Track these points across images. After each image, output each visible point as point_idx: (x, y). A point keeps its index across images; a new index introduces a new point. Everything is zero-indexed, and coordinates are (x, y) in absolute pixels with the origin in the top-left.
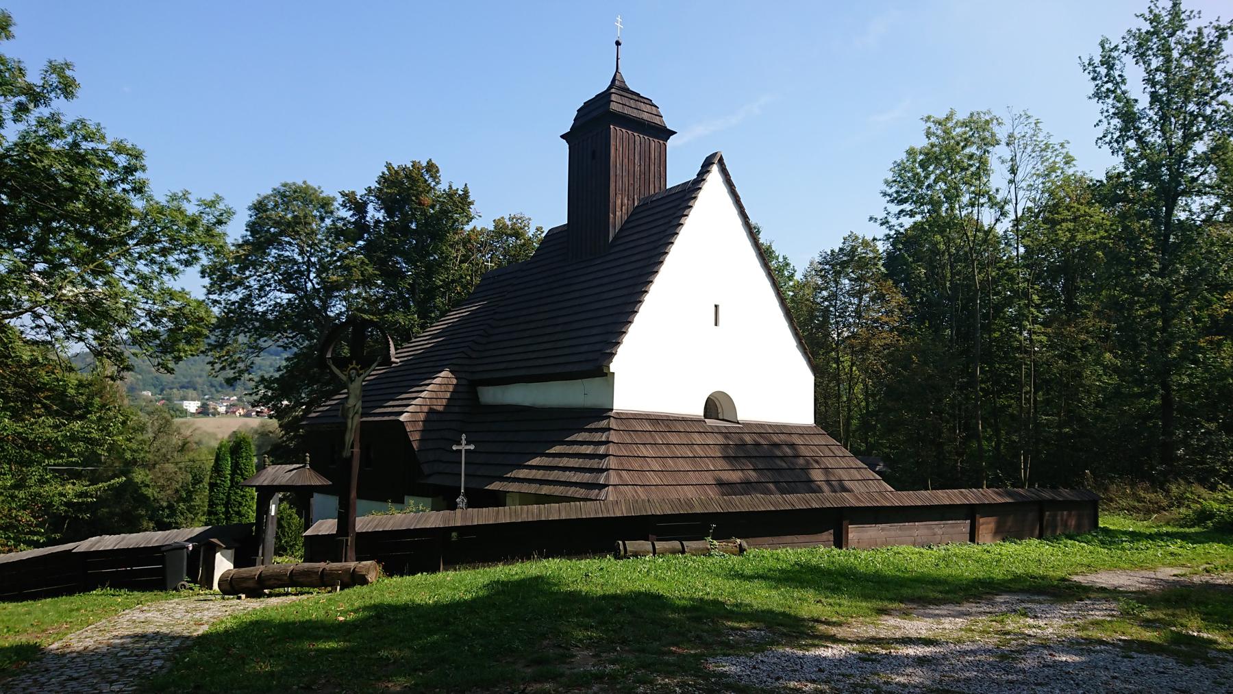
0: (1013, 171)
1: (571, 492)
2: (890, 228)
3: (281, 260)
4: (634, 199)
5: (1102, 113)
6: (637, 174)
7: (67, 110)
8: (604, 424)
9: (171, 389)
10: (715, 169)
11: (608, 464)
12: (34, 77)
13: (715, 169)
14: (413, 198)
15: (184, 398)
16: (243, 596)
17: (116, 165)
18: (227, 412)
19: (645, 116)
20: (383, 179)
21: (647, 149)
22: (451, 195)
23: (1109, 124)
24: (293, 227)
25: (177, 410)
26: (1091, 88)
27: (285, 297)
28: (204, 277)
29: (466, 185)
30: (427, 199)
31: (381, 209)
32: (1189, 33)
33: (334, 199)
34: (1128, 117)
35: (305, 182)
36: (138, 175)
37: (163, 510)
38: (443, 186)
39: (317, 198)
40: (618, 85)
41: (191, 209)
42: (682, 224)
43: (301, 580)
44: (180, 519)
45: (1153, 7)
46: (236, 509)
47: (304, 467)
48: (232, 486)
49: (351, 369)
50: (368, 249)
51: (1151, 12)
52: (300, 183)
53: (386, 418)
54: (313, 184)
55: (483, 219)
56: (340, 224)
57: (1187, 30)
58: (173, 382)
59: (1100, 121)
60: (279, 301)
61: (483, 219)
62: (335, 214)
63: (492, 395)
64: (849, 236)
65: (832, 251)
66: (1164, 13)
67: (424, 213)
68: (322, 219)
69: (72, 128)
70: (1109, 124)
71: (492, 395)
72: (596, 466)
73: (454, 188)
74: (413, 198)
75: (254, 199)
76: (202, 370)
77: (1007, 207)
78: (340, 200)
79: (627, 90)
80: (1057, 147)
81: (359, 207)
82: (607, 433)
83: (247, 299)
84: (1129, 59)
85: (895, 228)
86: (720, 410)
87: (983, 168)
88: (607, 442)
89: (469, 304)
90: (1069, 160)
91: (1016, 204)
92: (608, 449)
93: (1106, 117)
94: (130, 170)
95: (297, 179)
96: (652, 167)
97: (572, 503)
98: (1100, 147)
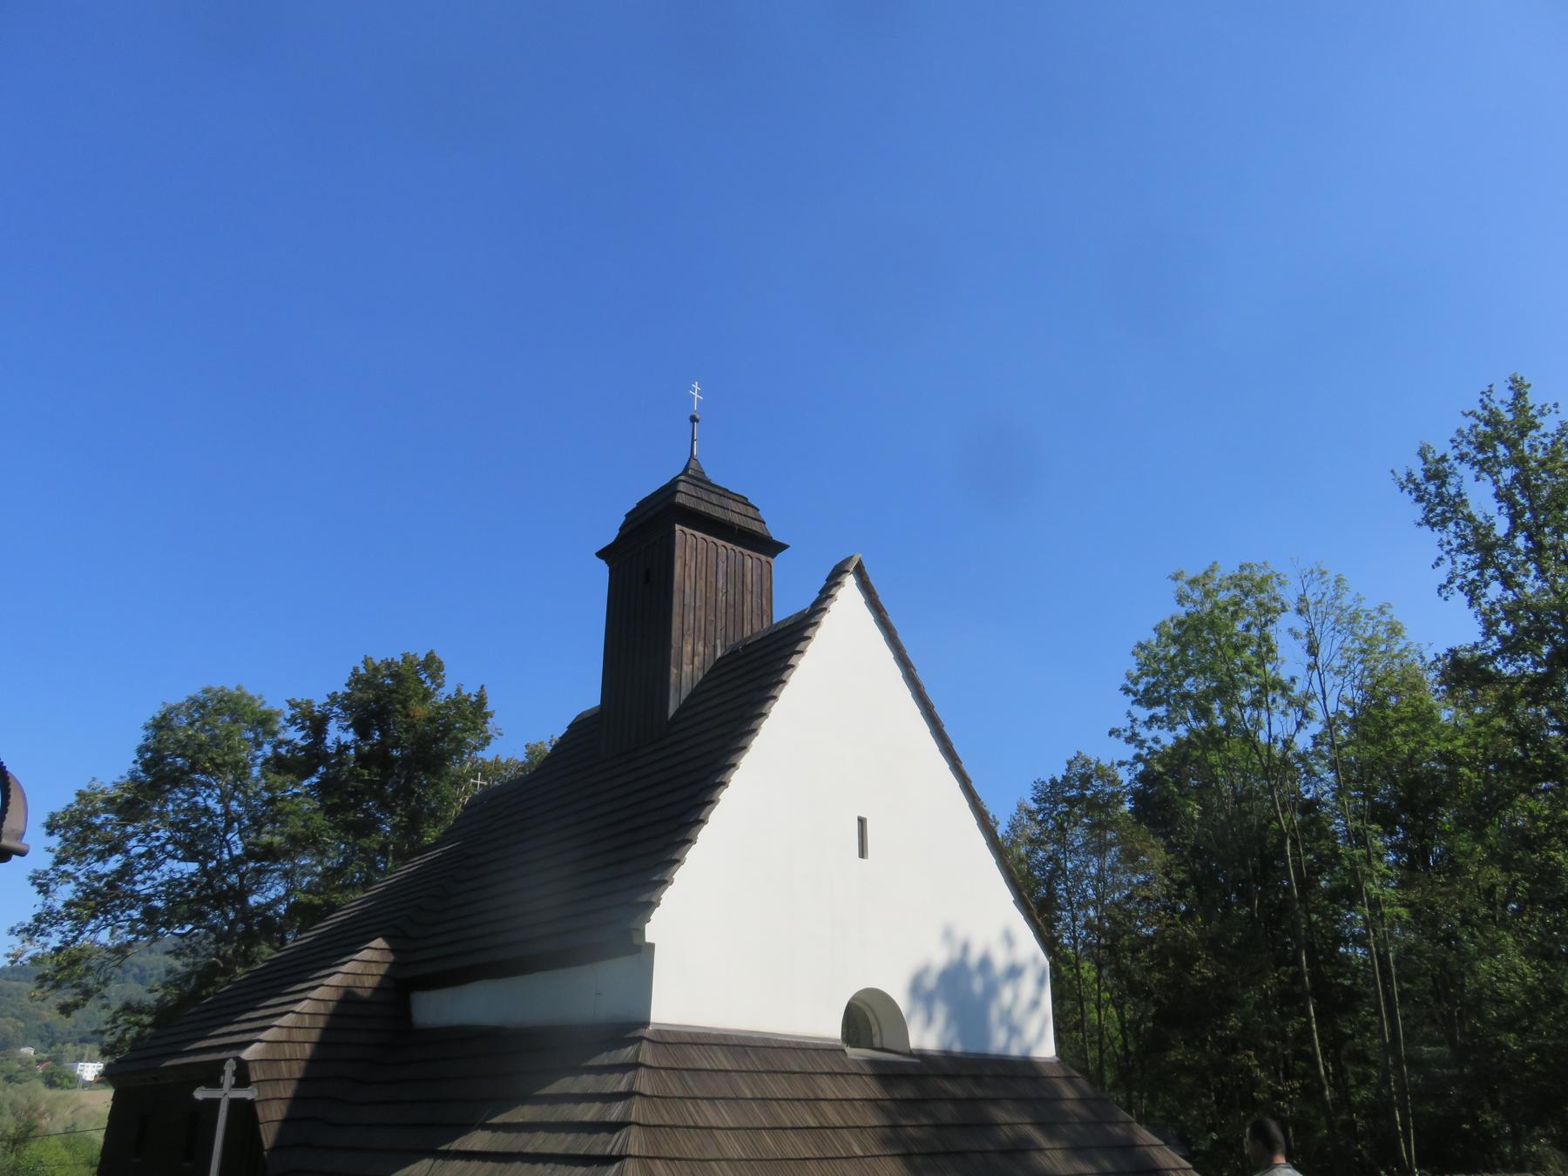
0: (1312, 650)
2: (1141, 744)
4: (715, 647)
5: (1441, 546)
6: (722, 606)
8: (627, 1054)
9: (64, 1043)
10: (850, 581)
11: (625, 1144)
13: (850, 581)
14: (398, 706)
15: (80, 1058)
19: (736, 519)
20: (356, 680)
21: (738, 568)
22: (457, 702)
23: (1454, 562)
25: (66, 1076)
26: (1418, 511)
28: (51, 834)
29: (482, 687)
30: (420, 711)
32: (1545, 435)
33: (278, 714)
34: (1484, 547)
35: (238, 688)
39: (253, 713)
42: (793, 666)
45: (1486, 400)
50: (324, 787)
51: (1484, 407)
54: (251, 690)
57: (1542, 430)
59: (1440, 559)
64: (1076, 758)
65: (1053, 781)
66: (1503, 409)
68: (259, 745)
70: (1454, 562)
72: (597, 1151)
73: (465, 692)
74: (398, 706)
75: (155, 711)
77: (1310, 705)
79: (709, 483)
80: (1374, 614)
81: (317, 726)
82: (630, 1074)
83: (126, 872)
84: (1464, 470)
85: (1147, 745)
86: (875, 1029)
87: (1266, 649)
88: (628, 1095)
89: (433, 850)
90: (1394, 631)
91: (1324, 699)
92: (627, 1111)
93: (1448, 553)
95: (226, 680)
96: (748, 598)
98: (1446, 599)
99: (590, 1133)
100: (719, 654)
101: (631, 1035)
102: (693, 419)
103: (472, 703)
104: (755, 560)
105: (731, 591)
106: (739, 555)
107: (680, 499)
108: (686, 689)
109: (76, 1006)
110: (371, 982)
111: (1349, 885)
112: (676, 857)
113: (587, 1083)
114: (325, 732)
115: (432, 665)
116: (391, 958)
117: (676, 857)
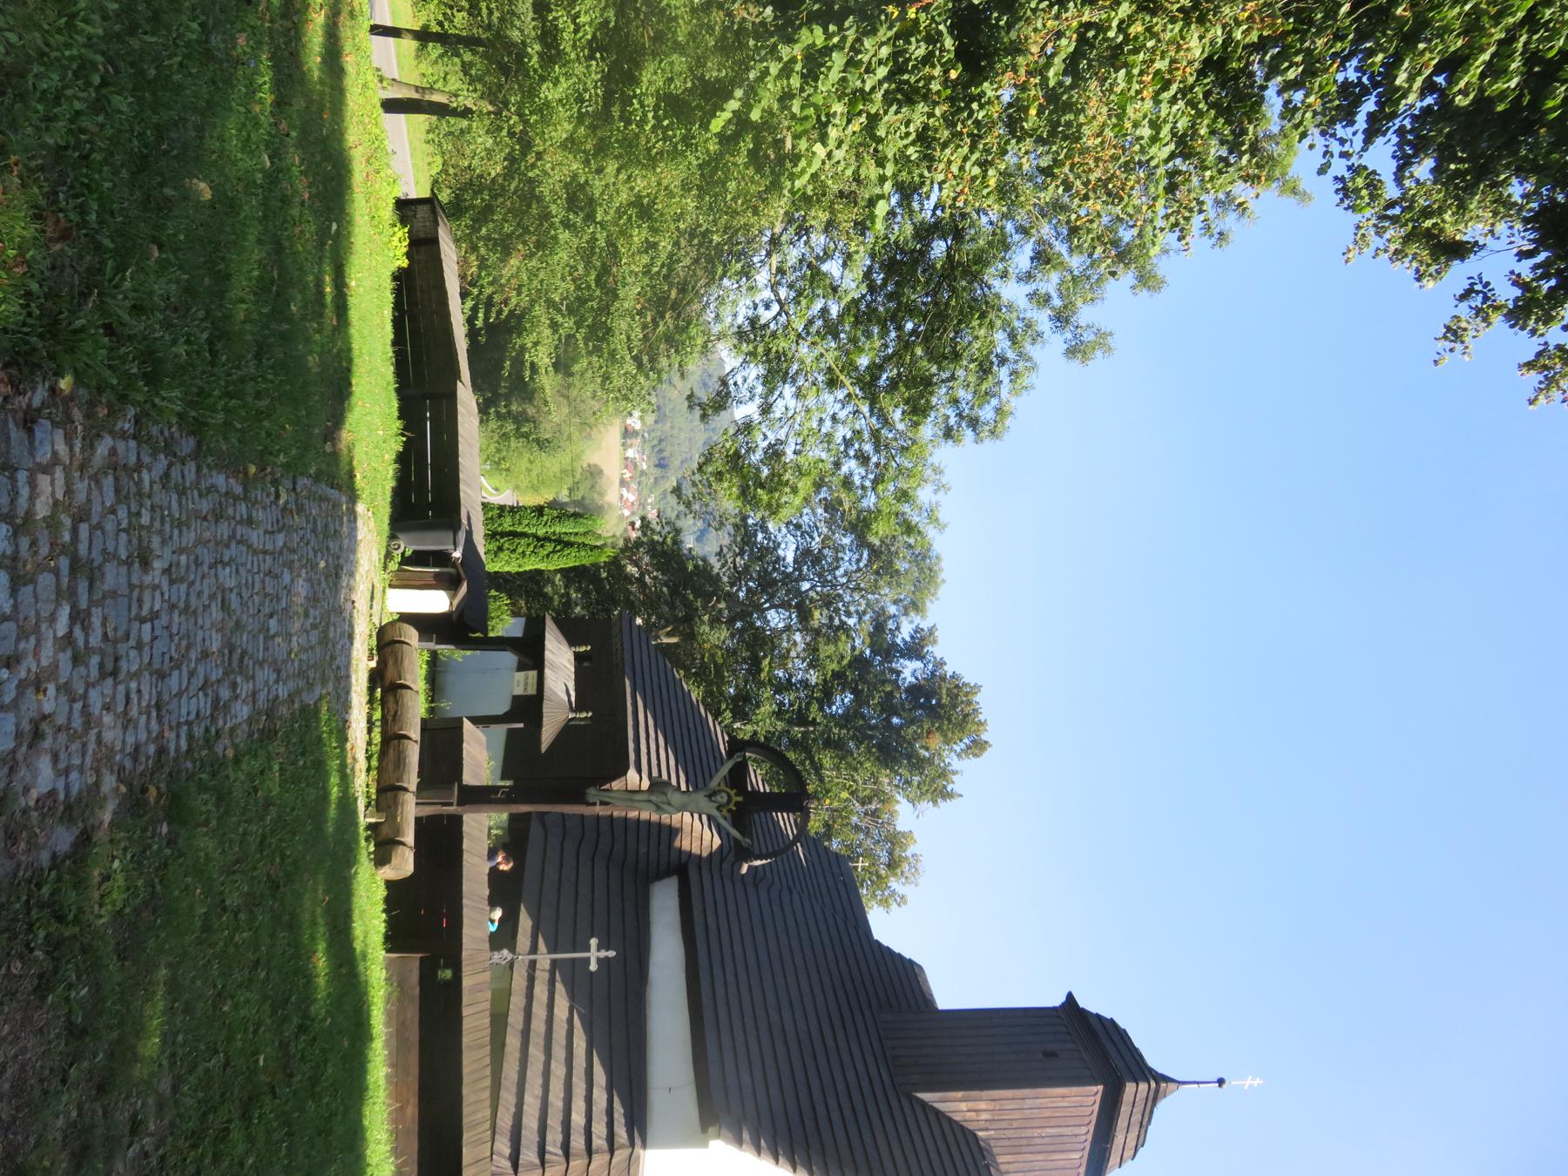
1: (508, 1098)
3: (838, 549)
4: (987, 1129)
6: (1028, 1133)
7: (1049, 350)
12: (1086, 314)
16: (373, 664)
17: (980, 407)
18: (626, 459)
22: (944, 774)
24: (881, 561)
27: (788, 553)
30: (936, 742)
31: (917, 678)
35: (944, 581)
36: (969, 433)
37: (505, 406)
38: (954, 762)
40: (1159, 1082)
41: (924, 495)
43: (391, 751)
44: (493, 424)
46: (506, 546)
47: (571, 709)
48: (539, 539)
49: (729, 795)
52: (942, 575)
53: (631, 746)
55: (906, 814)
56: (891, 625)
58: (664, 397)
60: (783, 546)
61: (906, 814)
62: (903, 619)
63: (664, 903)
67: (917, 737)
68: (895, 602)
69: (1022, 355)
71: (664, 903)
73: (954, 778)
76: (680, 429)
78: (925, 625)
81: (915, 649)
94: (974, 423)
96: (1040, 1157)
97: (488, 1071)
99: (562, 1123)
100: (980, 1134)
101: (636, 1134)
102: (1221, 1082)
103: (945, 787)
104: (1078, 1162)
105: (1043, 1141)
106: (1082, 1146)
107: (1130, 1088)
108: (940, 1106)
109: (679, 497)
110: (686, 846)
111: (1552, 200)
112: (781, 1159)
113: (600, 1097)
114: (910, 658)
115: (978, 747)
116: (705, 854)
117: (781, 1159)
